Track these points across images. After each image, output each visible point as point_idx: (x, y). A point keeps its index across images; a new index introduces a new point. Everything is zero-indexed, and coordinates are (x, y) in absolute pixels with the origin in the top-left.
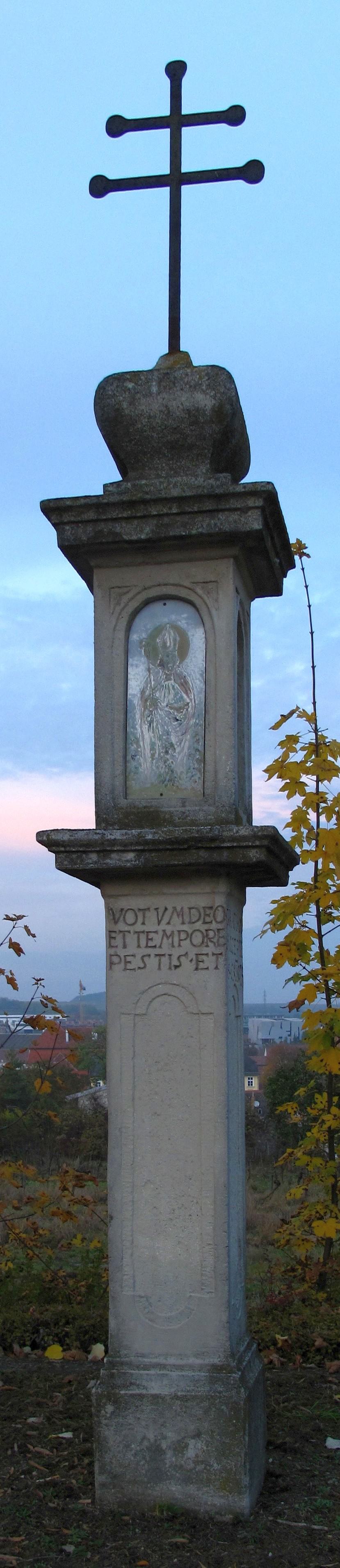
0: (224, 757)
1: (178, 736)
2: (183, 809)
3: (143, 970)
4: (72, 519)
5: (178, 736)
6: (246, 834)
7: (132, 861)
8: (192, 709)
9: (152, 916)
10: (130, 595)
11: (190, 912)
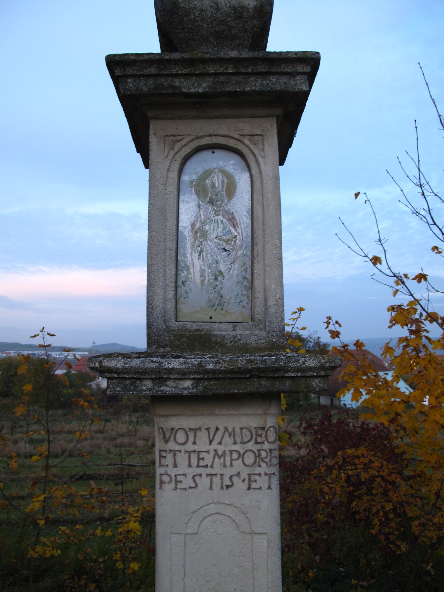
0: (273, 286)
1: (227, 265)
2: (234, 333)
3: (194, 490)
4: (135, 72)
5: (227, 265)
6: (314, 365)
7: (189, 389)
8: (240, 240)
9: (203, 436)
10: (183, 142)
11: (241, 433)
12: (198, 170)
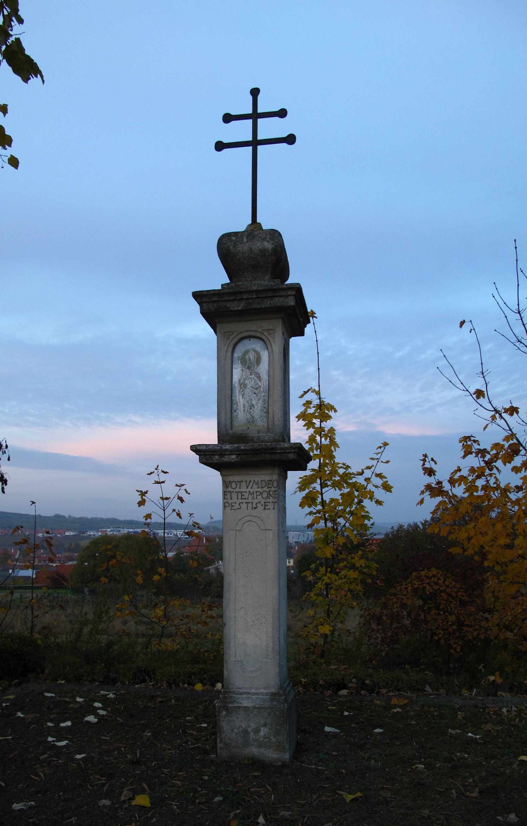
2: (258, 435)
3: (240, 510)
4: (207, 300)
9: (244, 485)
10: (233, 336)
12: (242, 350)
